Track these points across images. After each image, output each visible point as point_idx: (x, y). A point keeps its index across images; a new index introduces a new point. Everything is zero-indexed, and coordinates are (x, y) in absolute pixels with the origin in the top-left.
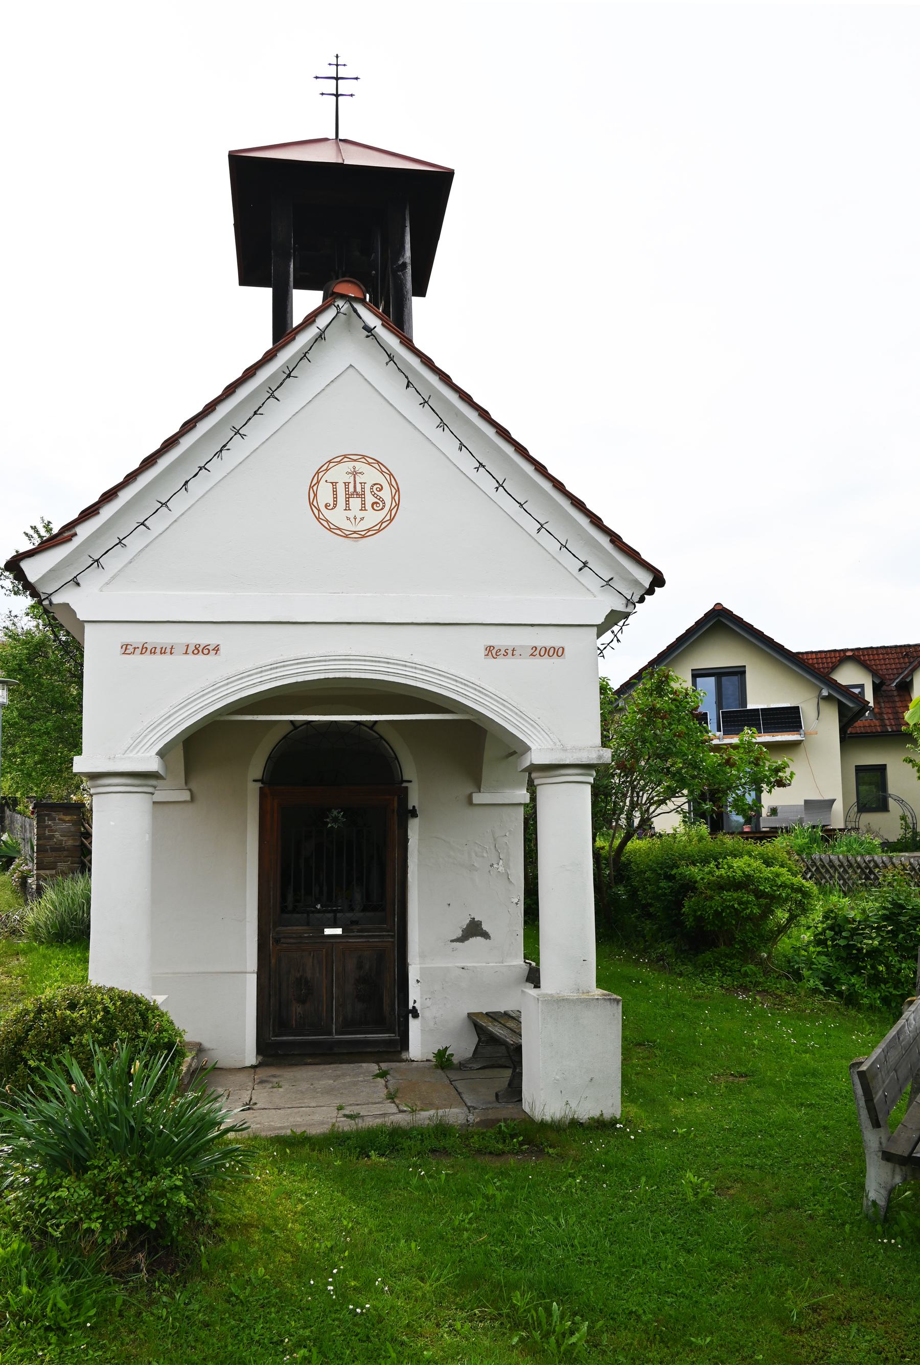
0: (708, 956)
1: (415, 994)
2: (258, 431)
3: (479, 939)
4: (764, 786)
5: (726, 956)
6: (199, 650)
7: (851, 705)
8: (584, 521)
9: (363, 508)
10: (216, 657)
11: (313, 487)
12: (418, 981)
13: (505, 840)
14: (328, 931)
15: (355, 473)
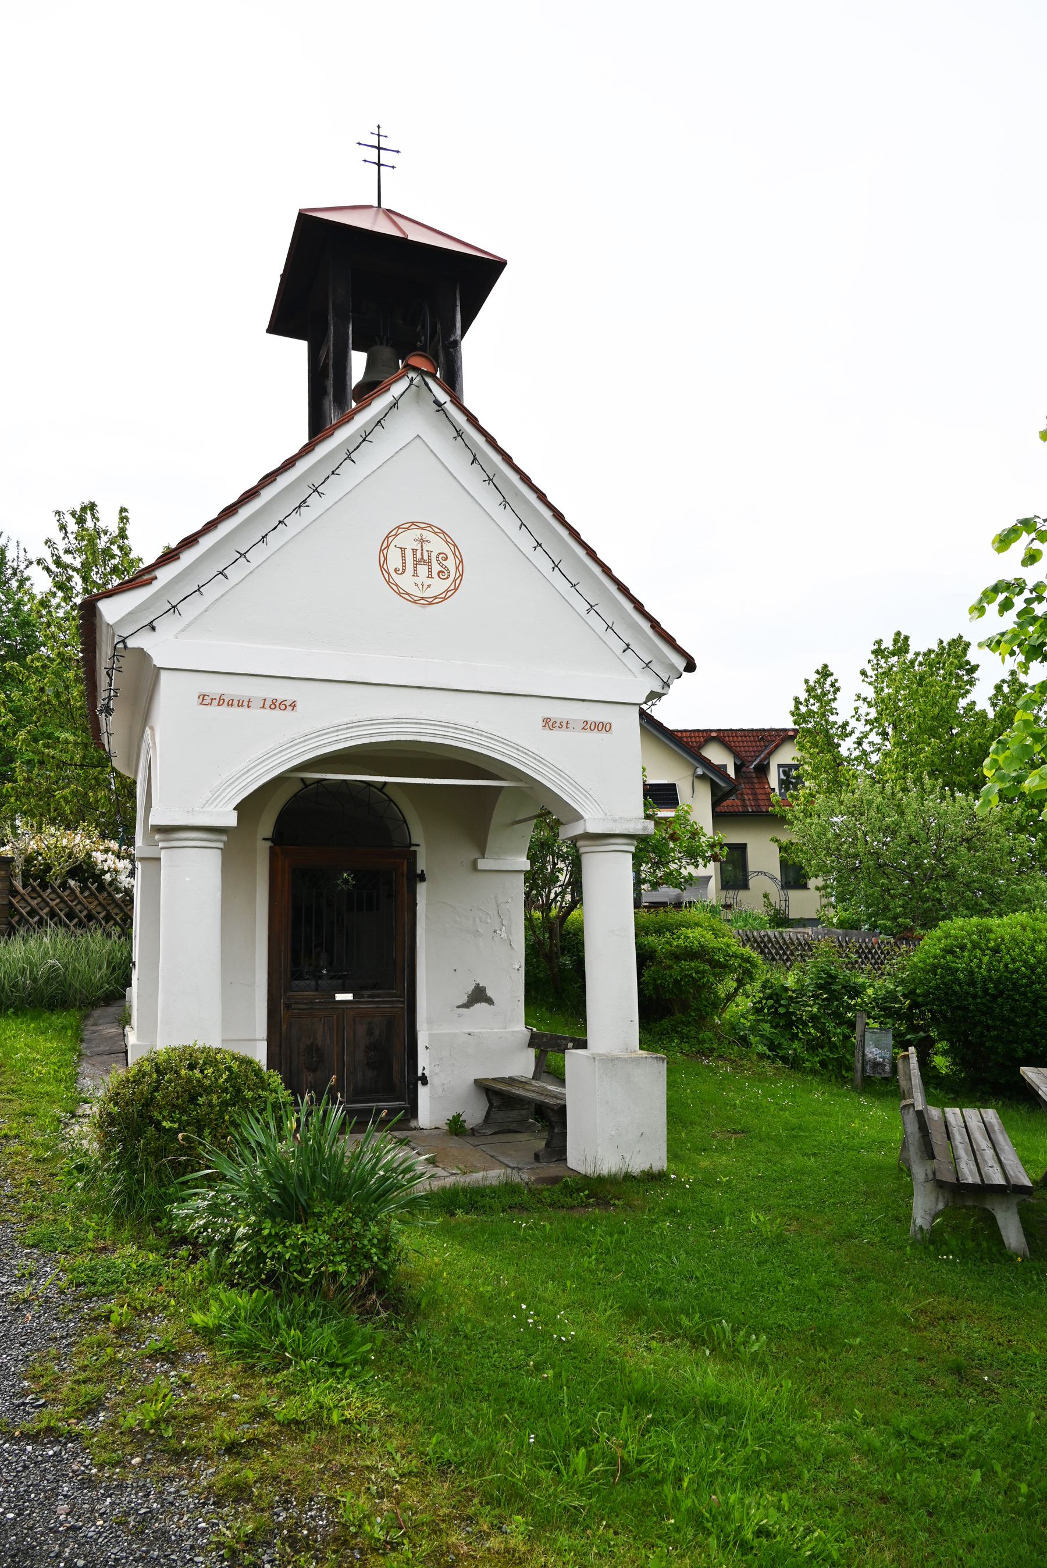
0: (665, 1023)
1: (424, 1061)
2: (334, 490)
3: (483, 1004)
4: (700, 860)
5: (683, 1023)
6: (276, 705)
7: (723, 785)
8: (629, 606)
9: (430, 576)
10: (293, 713)
11: (383, 550)
12: (427, 1048)
13: (507, 906)
14: (339, 997)
15: (422, 541)
